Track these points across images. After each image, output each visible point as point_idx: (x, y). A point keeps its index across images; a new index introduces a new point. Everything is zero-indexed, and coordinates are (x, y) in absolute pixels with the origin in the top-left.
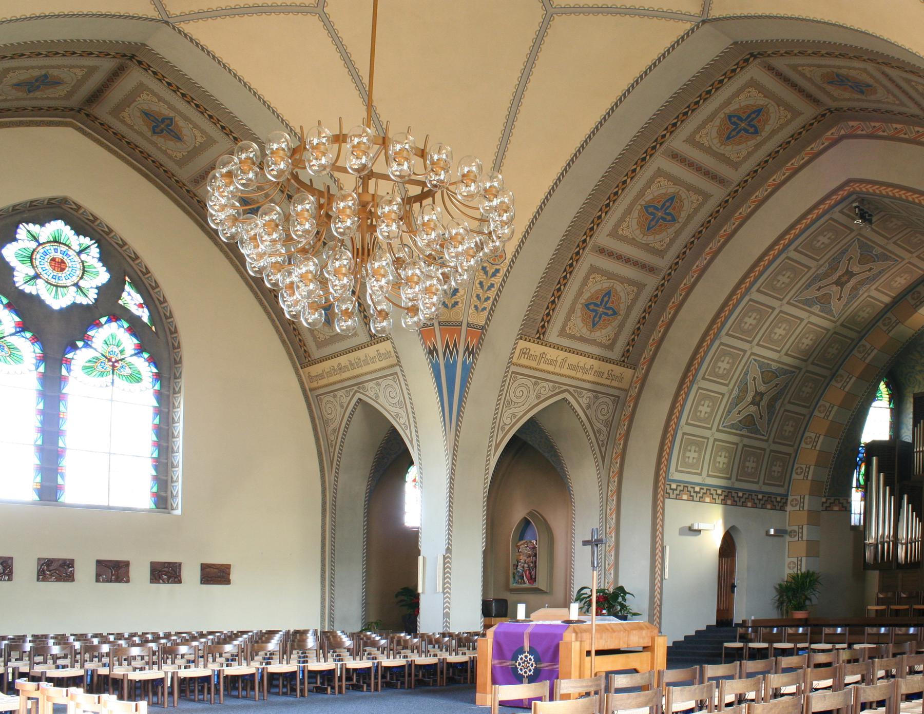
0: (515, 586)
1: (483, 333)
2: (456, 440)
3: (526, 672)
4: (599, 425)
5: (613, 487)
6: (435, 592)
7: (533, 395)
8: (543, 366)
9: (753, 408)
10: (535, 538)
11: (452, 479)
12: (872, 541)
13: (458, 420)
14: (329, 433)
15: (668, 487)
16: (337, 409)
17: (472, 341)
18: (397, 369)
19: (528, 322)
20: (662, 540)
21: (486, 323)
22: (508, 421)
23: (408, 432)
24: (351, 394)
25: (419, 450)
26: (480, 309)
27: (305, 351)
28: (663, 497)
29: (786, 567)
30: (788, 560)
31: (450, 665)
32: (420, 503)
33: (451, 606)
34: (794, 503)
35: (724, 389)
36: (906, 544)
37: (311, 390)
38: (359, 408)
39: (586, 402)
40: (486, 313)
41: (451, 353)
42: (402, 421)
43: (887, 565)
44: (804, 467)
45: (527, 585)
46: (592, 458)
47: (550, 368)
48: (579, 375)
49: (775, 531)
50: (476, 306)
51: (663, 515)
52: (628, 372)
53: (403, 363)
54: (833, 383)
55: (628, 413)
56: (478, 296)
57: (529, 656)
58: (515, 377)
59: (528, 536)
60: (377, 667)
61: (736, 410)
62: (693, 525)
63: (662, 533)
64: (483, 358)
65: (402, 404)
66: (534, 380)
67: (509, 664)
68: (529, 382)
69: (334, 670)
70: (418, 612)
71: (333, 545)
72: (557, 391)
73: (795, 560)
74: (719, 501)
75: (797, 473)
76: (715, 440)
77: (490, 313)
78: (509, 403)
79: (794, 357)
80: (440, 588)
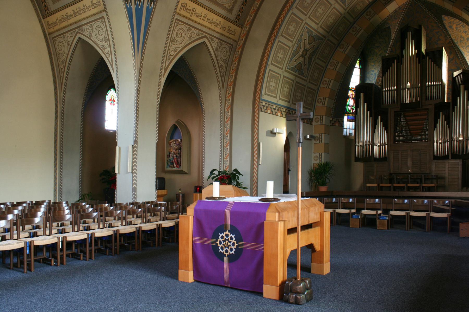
0: (169, 169)
2: (141, 62)
3: (227, 251)
4: (221, 62)
5: (228, 104)
6: (127, 172)
7: (187, 37)
8: (194, 18)
9: (302, 59)
10: (180, 138)
11: (138, 90)
12: (361, 144)
13: (143, 49)
14: (60, 64)
15: (261, 104)
16: (66, 46)
18: (104, 14)
20: (258, 138)
22: (172, 53)
23: (110, 59)
24: (74, 34)
25: (117, 71)
27: (45, 6)
28: (258, 110)
29: (313, 159)
30: (314, 155)
31: (144, 232)
32: (114, 115)
33: (138, 183)
34: (317, 120)
35: (290, 44)
36: (380, 146)
37: (49, 34)
38: (79, 45)
39: (216, 46)
42: (106, 51)
43: (368, 159)
44: (322, 98)
45: (176, 168)
46: (217, 84)
47: (198, 20)
48: (213, 27)
49: (310, 136)
51: (258, 122)
52: (239, 29)
53: (108, 10)
54: (338, 49)
55: (238, 56)
57: (230, 235)
58: (178, 23)
59: (176, 137)
60: (91, 237)
61: (294, 59)
62: (273, 129)
63: (258, 134)
65: (106, 39)
66: (188, 27)
67: (209, 241)
69: (56, 243)
70: (116, 188)
71: (62, 141)
72: (201, 36)
73: (318, 155)
74: (284, 116)
75: (318, 102)
76: (284, 77)
78: (173, 41)
79: (324, 30)
80: (130, 170)
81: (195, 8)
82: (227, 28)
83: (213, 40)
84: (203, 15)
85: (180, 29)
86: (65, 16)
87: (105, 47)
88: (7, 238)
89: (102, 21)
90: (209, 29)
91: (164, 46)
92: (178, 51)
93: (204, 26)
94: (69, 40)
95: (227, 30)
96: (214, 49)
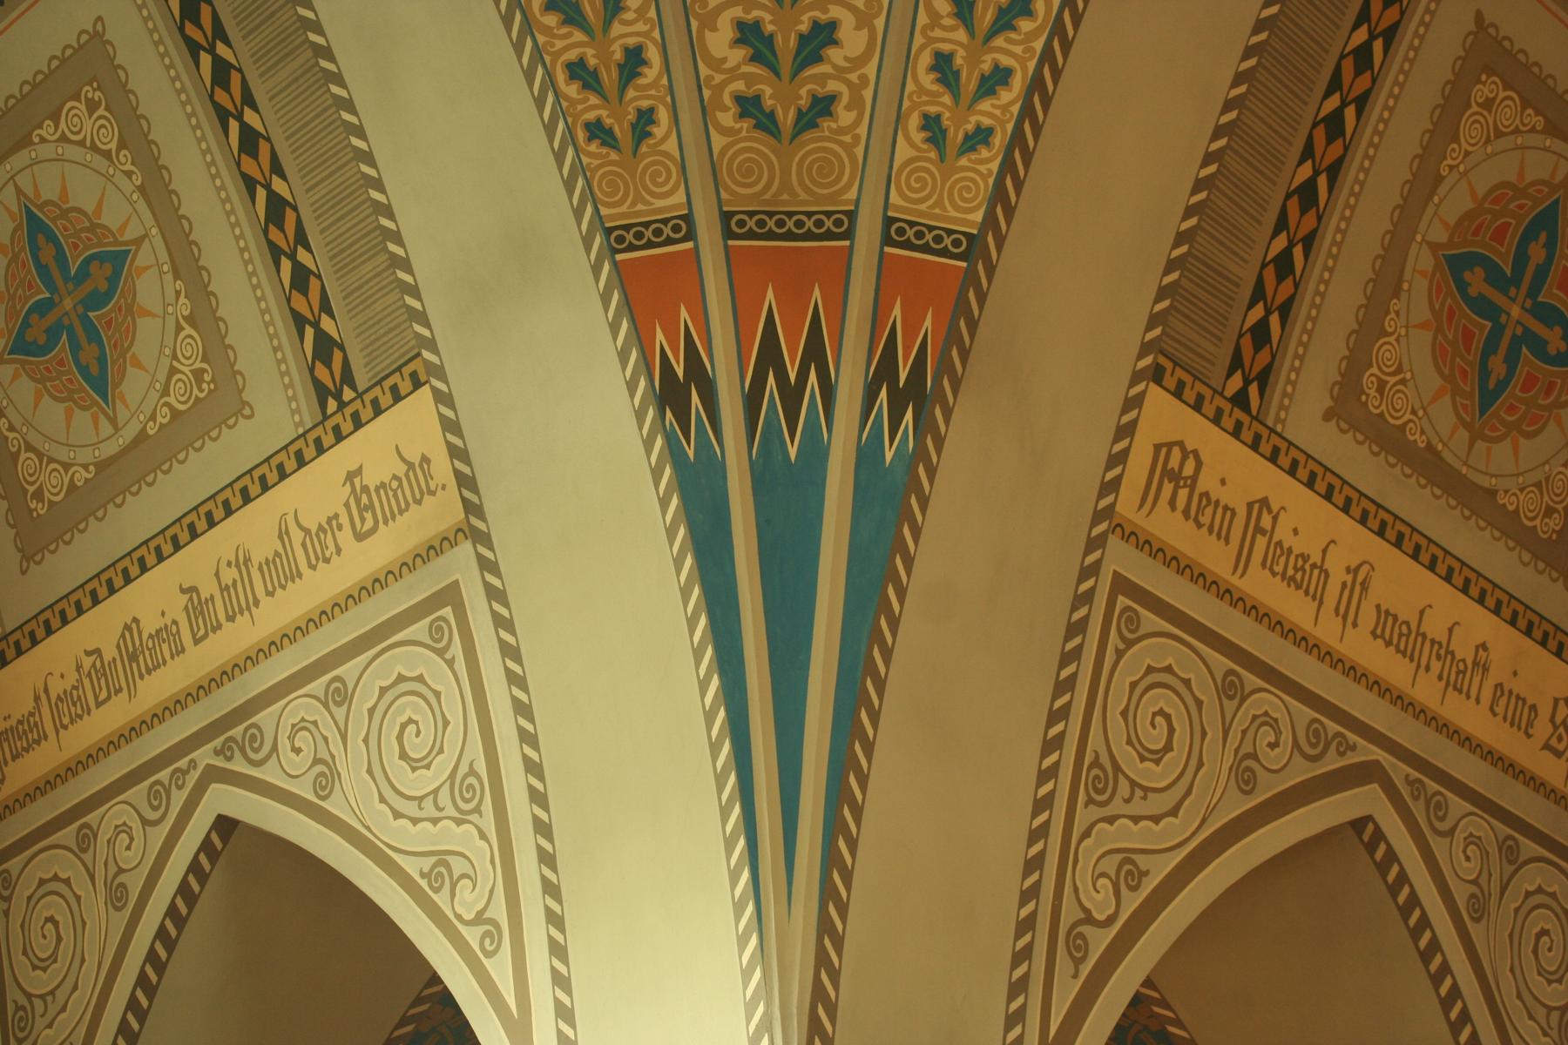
1: (971, 278)
2: (822, 960)
7: (1219, 760)
17: (912, 327)
18: (461, 563)
19: (1187, 284)
21: (990, 221)
22: (1100, 900)
26: (956, 136)
40: (989, 160)
41: (792, 396)
42: (467, 901)
47: (1294, 607)
48: (1426, 691)
50: (931, 124)
53: (497, 522)
56: (943, 65)
58: (1133, 620)
64: (972, 446)
65: (477, 790)
66: (1222, 663)
68: (1200, 668)
72: (1332, 763)
77: (1008, 166)
78: (1100, 779)
81: (1264, 502)
82: (1545, 711)
83: (1438, 808)
84: (1338, 576)
85: (1157, 677)
86: (109, 653)
87: (458, 866)
88: (1261, 450)
89: (436, 630)
90: (1400, 700)
91: (1021, 823)
92: (1149, 885)
93: (1353, 671)
94: (127, 858)
95: (1542, 729)
96: (1461, 894)
